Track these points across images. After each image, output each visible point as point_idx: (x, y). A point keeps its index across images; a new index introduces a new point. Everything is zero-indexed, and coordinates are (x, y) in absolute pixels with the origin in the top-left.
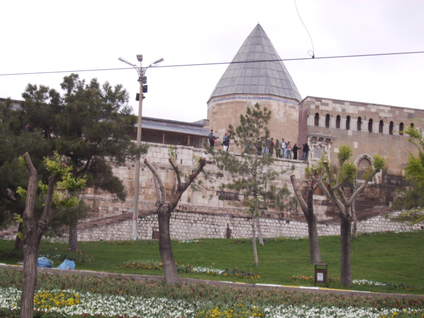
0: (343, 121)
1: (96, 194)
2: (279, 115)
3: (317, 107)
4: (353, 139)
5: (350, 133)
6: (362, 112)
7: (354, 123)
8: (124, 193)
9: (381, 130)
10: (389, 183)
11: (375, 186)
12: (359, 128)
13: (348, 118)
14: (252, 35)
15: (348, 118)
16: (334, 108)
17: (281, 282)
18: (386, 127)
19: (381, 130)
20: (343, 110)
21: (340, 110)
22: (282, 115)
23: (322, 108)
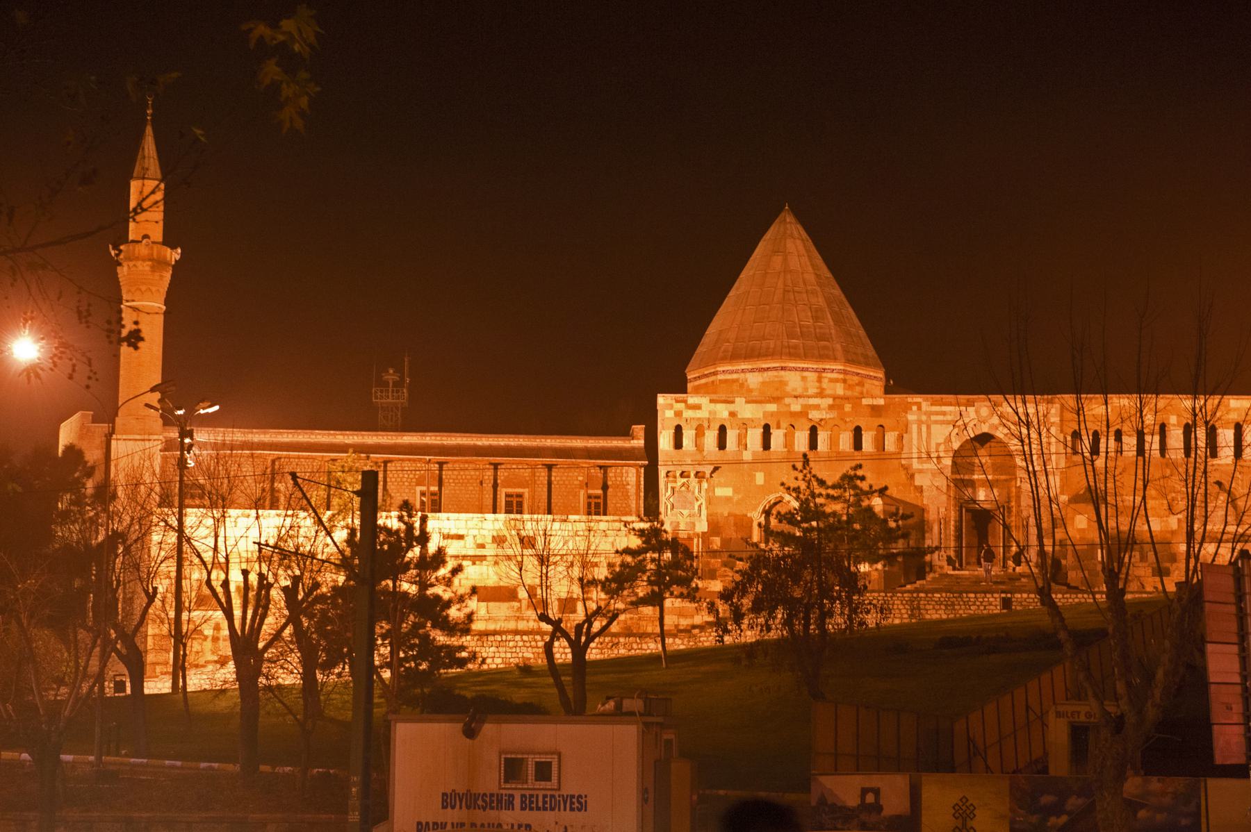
3: (678, 414)
6: (772, 414)
20: (733, 414)
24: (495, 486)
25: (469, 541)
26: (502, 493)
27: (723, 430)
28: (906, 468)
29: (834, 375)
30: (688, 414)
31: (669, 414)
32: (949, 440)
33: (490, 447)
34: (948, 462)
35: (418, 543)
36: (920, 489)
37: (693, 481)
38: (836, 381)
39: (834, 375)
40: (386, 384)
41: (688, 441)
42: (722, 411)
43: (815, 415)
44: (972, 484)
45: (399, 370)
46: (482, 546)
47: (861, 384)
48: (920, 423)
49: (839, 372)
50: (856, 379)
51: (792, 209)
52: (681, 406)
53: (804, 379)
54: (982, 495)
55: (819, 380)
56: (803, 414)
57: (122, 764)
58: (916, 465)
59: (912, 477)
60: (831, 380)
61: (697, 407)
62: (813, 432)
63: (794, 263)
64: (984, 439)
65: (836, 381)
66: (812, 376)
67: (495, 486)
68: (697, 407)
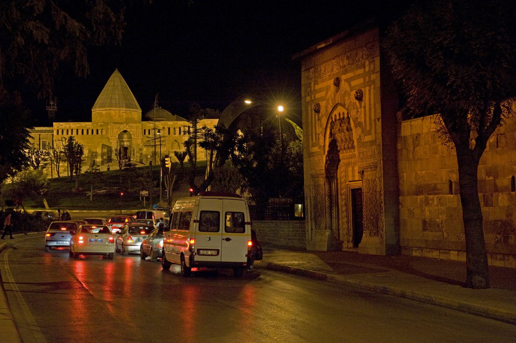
3: (58, 127)
20: (70, 127)
24: (40, 139)
26: (41, 141)
27: (68, 130)
28: (108, 138)
32: (117, 132)
33: (46, 130)
34: (117, 137)
35: (221, 143)
36: (111, 143)
40: (50, 105)
44: (123, 141)
45: (53, 101)
48: (111, 128)
51: (118, 70)
54: (125, 144)
63: (116, 83)
64: (125, 131)
67: (40, 139)
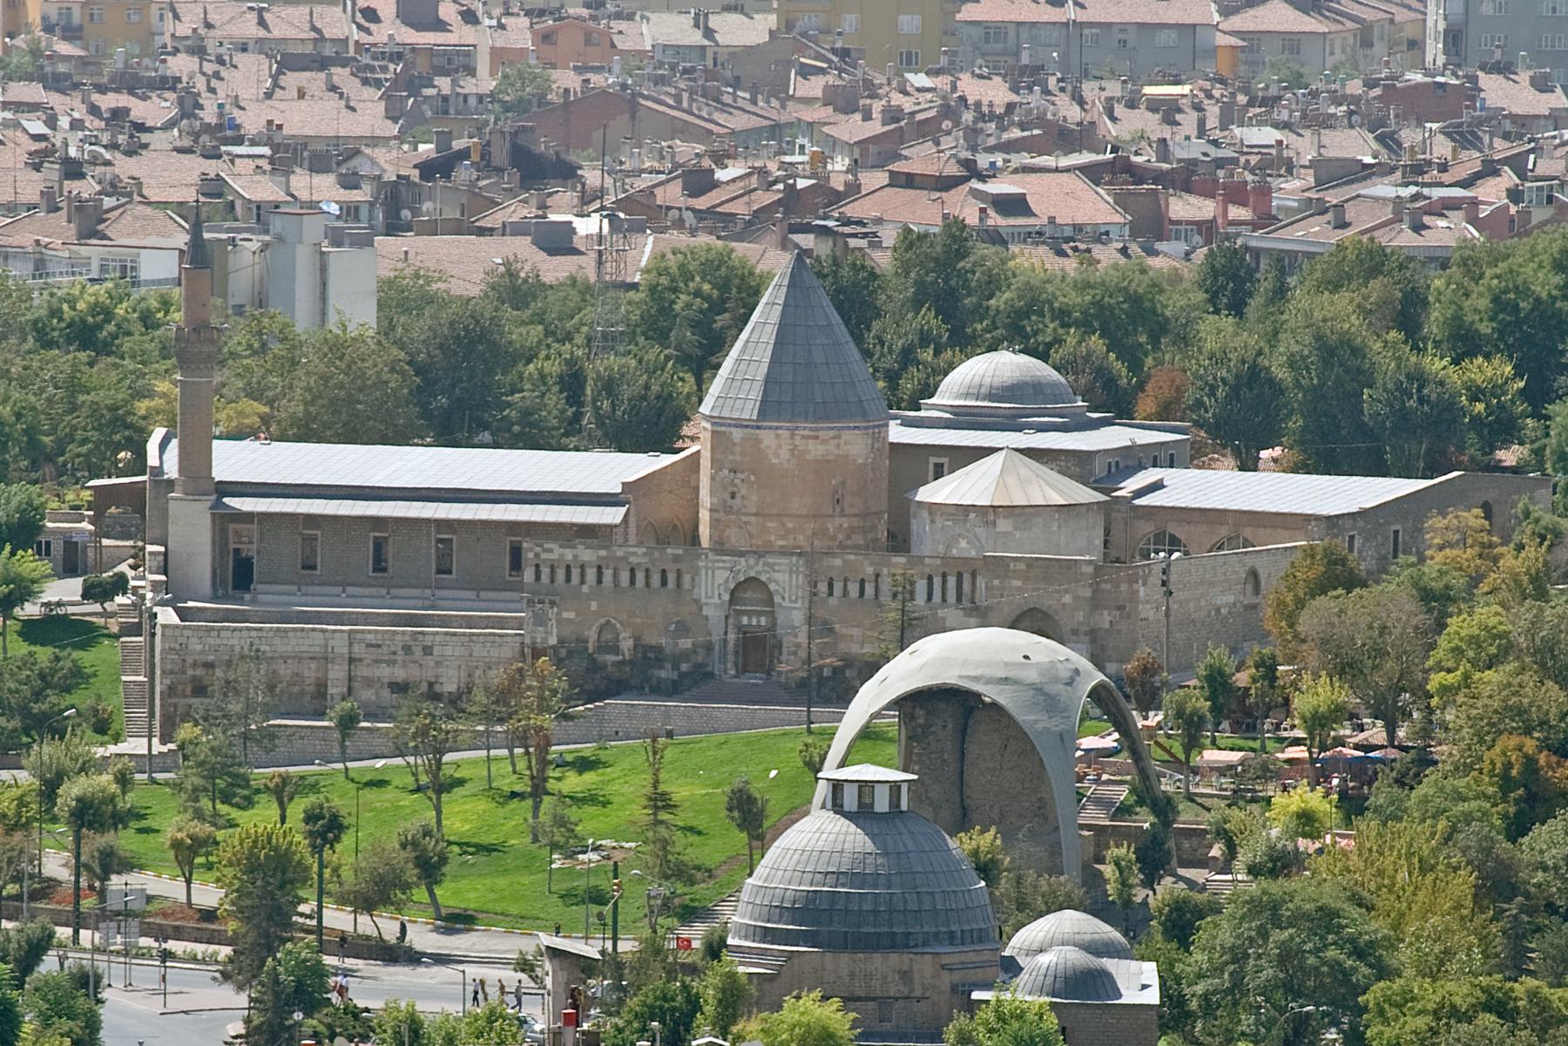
0: (575, 573)
1: (967, 160)
2: (778, 456)
3: (537, 555)
4: (589, 598)
5: (585, 589)
6: (604, 558)
7: (591, 574)
8: (525, 281)
9: (632, 582)
10: (645, 657)
11: (623, 662)
12: (599, 582)
13: (582, 567)
14: (486, 436)
15: (582, 567)
16: (562, 555)
17: (378, 729)
18: (640, 576)
19: (632, 582)
20: (575, 557)
21: (570, 557)
22: (784, 454)
23: (544, 556)
25: (385, 650)
27: (568, 567)
28: (697, 601)
29: (807, 433)
30: (544, 556)
31: (531, 555)
36: (707, 618)
37: (547, 606)
38: (809, 437)
39: (807, 433)
41: (545, 578)
42: (568, 554)
43: (633, 560)
46: (394, 653)
47: (838, 437)
48: (707, 568)
49: (811, 429)
50: (831, 433)
52: (538, 549)
53: (778, 436)
55: (792, 437)
56: (625, 558)
57: (737, 653)
58: (704, 600)
59: (701, 609)
60: (803, 437)
61: (551, 551)
62: (632, 571)
65: (809, 437)
66: (785, 434)
68: (551, 551)
